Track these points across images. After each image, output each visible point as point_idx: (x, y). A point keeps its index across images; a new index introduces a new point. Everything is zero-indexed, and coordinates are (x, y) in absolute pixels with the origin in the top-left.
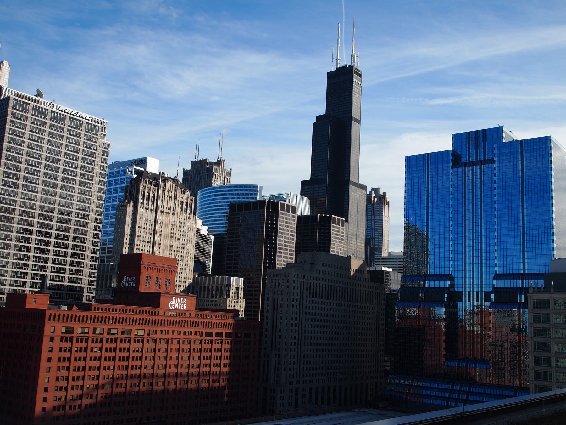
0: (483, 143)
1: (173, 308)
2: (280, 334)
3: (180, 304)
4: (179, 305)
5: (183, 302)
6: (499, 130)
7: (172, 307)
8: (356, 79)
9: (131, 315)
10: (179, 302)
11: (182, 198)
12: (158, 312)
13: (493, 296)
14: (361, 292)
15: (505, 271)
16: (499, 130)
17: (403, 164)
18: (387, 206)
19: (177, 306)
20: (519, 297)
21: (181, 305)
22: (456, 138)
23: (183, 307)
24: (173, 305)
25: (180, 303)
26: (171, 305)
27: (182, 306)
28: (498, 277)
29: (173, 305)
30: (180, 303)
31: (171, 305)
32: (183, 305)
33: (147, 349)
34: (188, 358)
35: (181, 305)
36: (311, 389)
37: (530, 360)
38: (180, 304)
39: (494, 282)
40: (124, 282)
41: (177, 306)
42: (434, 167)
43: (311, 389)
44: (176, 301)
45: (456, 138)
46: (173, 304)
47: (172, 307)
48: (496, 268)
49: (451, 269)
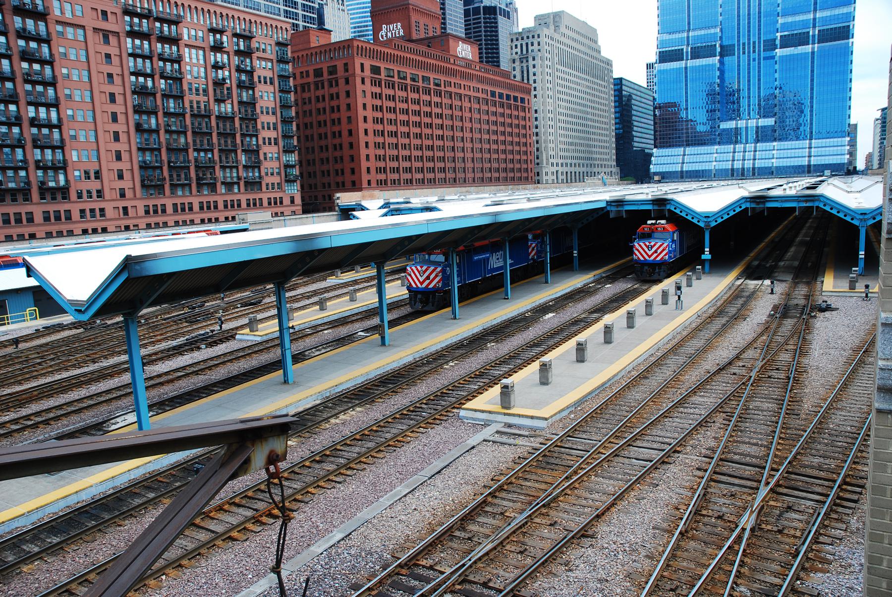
2: (115, 127)
4: (392, 34)
5: (397, 27)
8: (501, 20)
9: (96, 203)
10: (392, 29)
12: (102, 210)
18: (515, 14)
19: (389, 35)
21: (395, 33)
23: (399, 34)
26: (382, 36)
31: (382, 36)
35: (395, 33)
36: (521, 45)
37: (605, 163)
38: (393, 32)
40: (383, 33)
41: (389, 35)
42: (788, 75)
43: (521, 45)
46: (384, 34)
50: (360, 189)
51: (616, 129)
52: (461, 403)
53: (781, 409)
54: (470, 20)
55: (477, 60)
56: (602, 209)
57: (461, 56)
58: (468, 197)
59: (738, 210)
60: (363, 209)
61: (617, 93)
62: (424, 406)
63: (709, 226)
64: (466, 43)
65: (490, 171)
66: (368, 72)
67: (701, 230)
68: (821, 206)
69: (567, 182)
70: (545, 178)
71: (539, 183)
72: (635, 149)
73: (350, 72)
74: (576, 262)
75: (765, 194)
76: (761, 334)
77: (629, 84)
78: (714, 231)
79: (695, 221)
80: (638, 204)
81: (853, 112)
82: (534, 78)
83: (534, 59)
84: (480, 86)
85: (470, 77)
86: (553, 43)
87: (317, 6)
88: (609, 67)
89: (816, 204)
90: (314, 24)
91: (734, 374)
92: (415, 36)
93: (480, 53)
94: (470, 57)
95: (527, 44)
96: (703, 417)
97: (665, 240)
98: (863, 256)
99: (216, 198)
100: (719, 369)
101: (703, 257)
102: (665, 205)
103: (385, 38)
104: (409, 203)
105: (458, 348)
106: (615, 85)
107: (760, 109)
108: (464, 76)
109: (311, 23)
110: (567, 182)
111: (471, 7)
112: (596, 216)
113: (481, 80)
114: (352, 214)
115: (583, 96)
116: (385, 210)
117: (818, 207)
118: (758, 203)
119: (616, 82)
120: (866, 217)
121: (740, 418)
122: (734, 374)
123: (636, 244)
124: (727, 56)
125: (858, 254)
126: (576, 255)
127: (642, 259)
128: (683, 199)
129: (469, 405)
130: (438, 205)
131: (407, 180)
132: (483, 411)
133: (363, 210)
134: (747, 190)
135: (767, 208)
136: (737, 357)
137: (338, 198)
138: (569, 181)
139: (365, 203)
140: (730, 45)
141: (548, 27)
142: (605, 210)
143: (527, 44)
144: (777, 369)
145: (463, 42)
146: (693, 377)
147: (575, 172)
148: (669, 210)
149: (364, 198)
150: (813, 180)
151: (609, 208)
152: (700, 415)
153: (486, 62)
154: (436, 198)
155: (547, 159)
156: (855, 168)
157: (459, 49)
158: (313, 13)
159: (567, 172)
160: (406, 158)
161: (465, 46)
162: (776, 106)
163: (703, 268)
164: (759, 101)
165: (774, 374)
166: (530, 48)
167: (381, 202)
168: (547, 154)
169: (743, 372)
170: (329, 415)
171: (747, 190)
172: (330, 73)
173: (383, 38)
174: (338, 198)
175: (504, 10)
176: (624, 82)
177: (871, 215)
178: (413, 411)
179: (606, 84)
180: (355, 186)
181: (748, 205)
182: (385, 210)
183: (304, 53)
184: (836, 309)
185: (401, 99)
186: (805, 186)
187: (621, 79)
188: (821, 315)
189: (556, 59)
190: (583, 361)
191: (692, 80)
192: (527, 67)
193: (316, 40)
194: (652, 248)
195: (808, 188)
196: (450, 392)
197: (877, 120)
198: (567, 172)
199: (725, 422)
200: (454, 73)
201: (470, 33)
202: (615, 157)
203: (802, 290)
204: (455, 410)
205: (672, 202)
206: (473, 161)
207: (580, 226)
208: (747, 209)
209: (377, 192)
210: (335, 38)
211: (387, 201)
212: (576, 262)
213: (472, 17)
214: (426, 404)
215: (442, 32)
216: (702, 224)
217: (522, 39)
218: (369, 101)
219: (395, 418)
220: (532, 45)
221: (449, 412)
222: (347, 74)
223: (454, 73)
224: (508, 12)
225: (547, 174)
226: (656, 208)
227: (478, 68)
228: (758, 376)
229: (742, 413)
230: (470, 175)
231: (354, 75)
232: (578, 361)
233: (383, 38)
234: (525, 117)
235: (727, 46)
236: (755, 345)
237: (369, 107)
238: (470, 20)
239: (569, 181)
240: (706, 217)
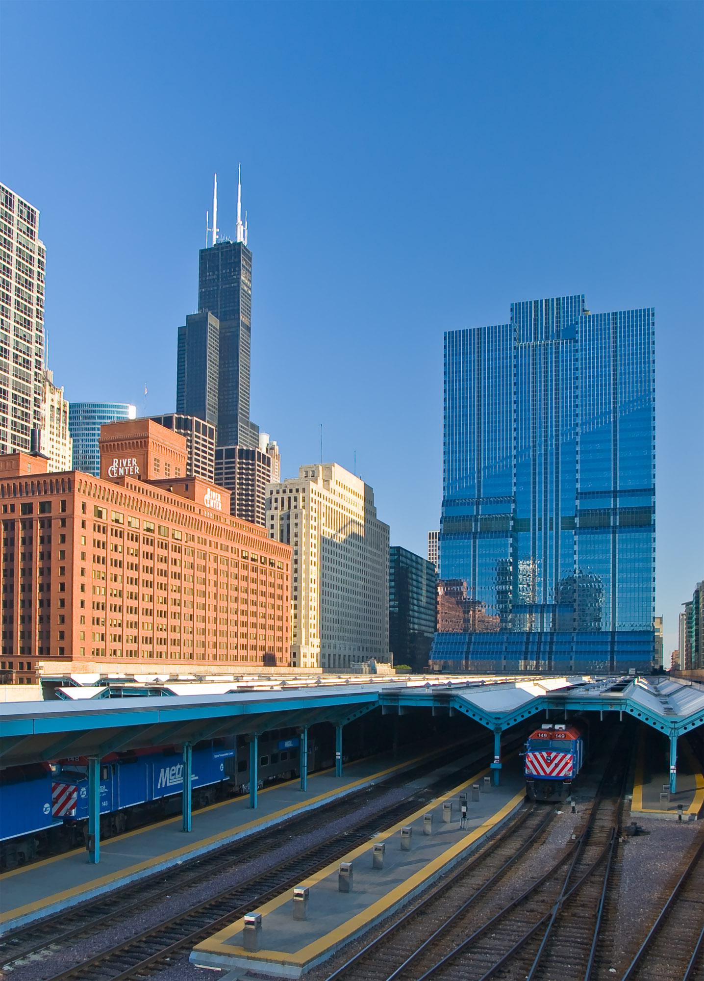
0: (220, 969)
1: (116, 475)
3: (127, 468)
4: (125, 470)
6: (578, 300)
7: (113, 475)
11: (52, 400)
13: (577, 520)
14: (334, 659)
15: (590, 486)
16: (578, 300)
17: (440, 343)
20: (473, 526)
21: (129, 470)
22: (519, 310)
24: (115, 472)
25: (127, 466)
26: (112, 472)
27: (131, 470)
28: (583, 495)
29: (115, 472)
30: (127, 466)
32: (134, 469)
33: (83, 538)
34: (150, 625)
35: (129, 470)
36: (283, 499)
38: (127, 468)
39: (578, 502)
40: (114, 468)
41: (121, 471)
43: (283, 499)
44: (119, 464)
45: (519, 310)
46: (115, 469)
47: (113, 475)
48: (578, 486)
49: (514, 489)
50: (70, 659)
51: (390, 607)
52: (191, 942)
53: (588, 955)
54: (221, 463)
55: (229, 512)
56: (373, 703)
57: (208, 506)
58: (62, 676)
59: (534, 712)
60: (72, 684)
61: (393, 564)
62: (143, 945)
63: (501, 728)
64: (215, 491)
65: (236, 648)
66: (90, 515)
67: (490, 735)
68: (457, 707)
69: (329, 667)
70: (302, 660)
71: (295, 666)
72: (412, 631)
73: (68, 512)
74: (339, 766)
75: (565, 694)
76: (563, 862)
77: (407, 555)
78: (505, 734)
79: (483, 723)
80: (416, 700)
81: (657, 604)
82: (295, 539)
83: (296, 517)
84: (230, 544)
85: (218, 532)
86: (321, 500)
87: (32, 427)
88: (385, 534)
89: (623, 708)
90: (26, 448)
91: (532, 911)
92: (153, 476)
93: (232, 504)
94: (220, 508)
95: (289, 498)
96: (495, 965)
97: (567, 752)
98: (675, 771)
99: (11, 660)
100: (514, 904)
101: (493, 766)
102: (448, 702)
103: (116, 475)
104: (135, 681)
105: (188, 869)
106: (391, 555)
107: (557, 593)
108: (210, 529)
109: (22, 446)
110: (329, 667)
111: (224, 448)
112: (365, 711)
113: (231, 536)
114: (59, 690)
115: (354, 565)
116: (101, 689)
117: (624, 713)
118: (557, 704)
119: (392, 551)
120: (677, 726)
121: (540, 966)
122: (532, 911)
123: (530, 754)
124: (521, 530)
125: (669, 769)
126: (339, 757)
127: (535, 773)
128: (470, 696)
129: (202, 945)
130: (173, 687)
131: (131, 651)
132: (220, 954)
133: (73, 686)
134: (544, 688)
135: (568, 710)
136: (536, 891)
137: (41, 668)
138: (332, 666)
139: (75, 677)
140: (525, 520)
141: (316, 481)
142: (377, 705)
143: (289, 498)
144: (583, 906)
145: (212, 490)
146: (482, 916)
147: (340, 655)
148: (454, 709)
149: (75, 670)
150: (619, 679)
151: (381, 703)
152: (492, 962)
153: (238, 515)
154: (167, 677)
155: (307, 638)
156: (662, 667)
157: (207, 497)
158: (26, 434)
159: (329, 655)
160: (131, 623)
161: (214, 494)
162: (575, 591)
163: (492, 779)
164: (557, 584)
165: (579, 911)
166: (293, 504)
167: (96, 678)
168: (307, 631)
169: (542, 908)
170: (14, 955)
171: (544, 688)
172: (43, 510)
173: (113, 474)
174: (41, 668)
175: (264, 456)
176: (401, 551)
177: (682, 724)
178: (128, 952)
179: (381, 553)
180: (65, 655)
181: (545, 706)
182: (101, 689)
183: (11, 482)
184: (648, 833)
185: (131, 551)
186: (608, 687)
187: (399, 549)
188: (635, 841)
189: (323, 520)
190: (347, 891)
191: (481, 556)
192: (288, 526)
193: (28, 467)
194: (552, 761)
195: (613, 690)
196: (177, 927)
197: (682, 615)
198: (329, 655)
199: (522, 972)
200: (198, 525)
201: (221, 479)
202: (388, 640)
203: (608, 807)
204: (184, 952)
205: (457, 699)
206: (215, 634)
207: (346, 722)
208: (544, 711)
209: (91, 665)
210: (52, 467)
211: (104, 677)
212: (339, 766)
213: (224, 461)
214: (145, 942)
215: (187, 475)
216: (491, 727)
217: (284, 492)
218: (91, 551)
219: (104, 960)
220: (296, 499)
221: (176, 953)
222: (63, 514)
223: (198, 525)
224: (269, 459)
225: (305, 656)
226: (438, 704)
227: (228, 522)
228: (560, 914)
229: (542, 961)
230: (211, 651)
231: (72, 517)
232: (340, 890)
233: (113, 474)
234: (282, 586)
235: (522, 520)
236: (556, 876)
237: (89, 557)
238: (221, 463)
239: (332, 666)
240: (496, 718)
